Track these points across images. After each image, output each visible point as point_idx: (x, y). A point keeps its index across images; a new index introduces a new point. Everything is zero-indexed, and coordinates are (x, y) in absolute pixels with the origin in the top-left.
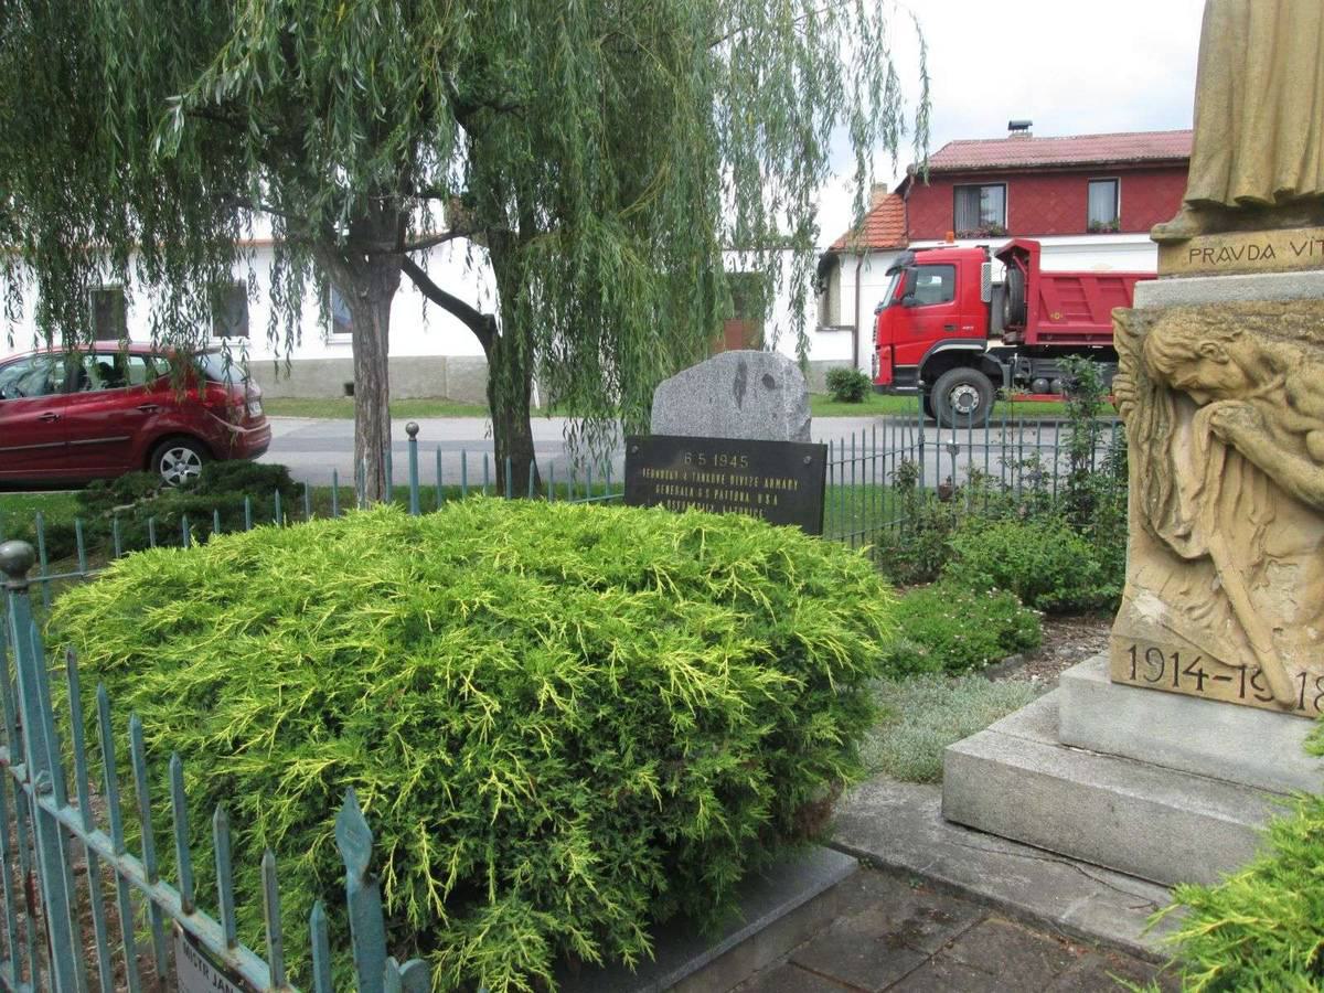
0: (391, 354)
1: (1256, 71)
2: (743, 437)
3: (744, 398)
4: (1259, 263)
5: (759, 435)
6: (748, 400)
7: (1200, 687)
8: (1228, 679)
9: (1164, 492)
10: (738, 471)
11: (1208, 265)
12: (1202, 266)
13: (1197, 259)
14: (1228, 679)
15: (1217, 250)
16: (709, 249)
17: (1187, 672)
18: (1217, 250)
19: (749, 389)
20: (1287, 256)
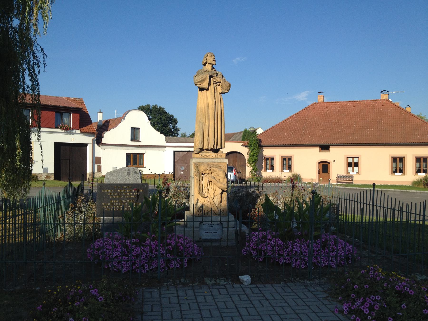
0: (32, 173)
1: (41, 197)
2: (130, 183)
3: (130, 175)
4: (208, 157)
5: (134, 182)
6: (131, 176)
7: (208, 215)
8: (384, 193)
9: (202, 189)
10: (128, 189)
11: (201, 157)
12: (201, 157)
13: (200, 156)
14: (384, 193)
15: (203, 155)
16: (7, 204)
17: (206, 213)
18: (203, 155)
19: (131, 174)
20: (211, 157)
